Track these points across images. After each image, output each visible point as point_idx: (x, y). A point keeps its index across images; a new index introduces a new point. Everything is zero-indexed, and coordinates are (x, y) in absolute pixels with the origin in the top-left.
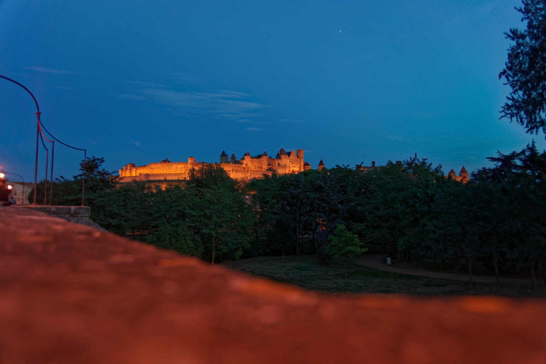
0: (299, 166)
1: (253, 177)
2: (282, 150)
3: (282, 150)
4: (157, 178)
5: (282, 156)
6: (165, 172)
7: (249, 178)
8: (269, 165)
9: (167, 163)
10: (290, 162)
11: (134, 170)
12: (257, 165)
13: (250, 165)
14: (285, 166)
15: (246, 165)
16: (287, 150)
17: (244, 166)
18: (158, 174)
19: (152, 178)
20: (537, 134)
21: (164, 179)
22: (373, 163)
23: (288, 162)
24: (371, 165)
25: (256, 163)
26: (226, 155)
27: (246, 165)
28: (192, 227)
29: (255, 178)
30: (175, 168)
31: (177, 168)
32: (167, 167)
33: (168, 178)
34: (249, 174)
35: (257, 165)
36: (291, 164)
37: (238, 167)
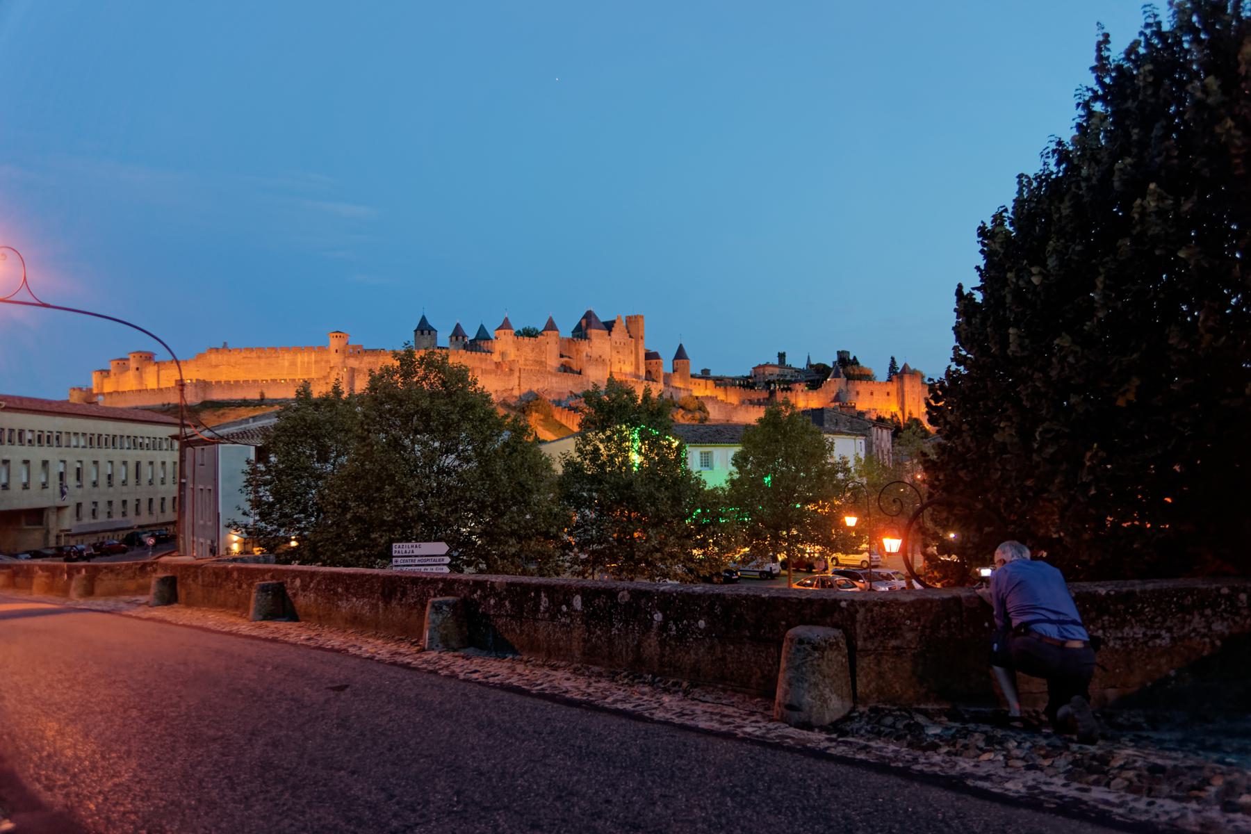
0: (633, 358)
1: (525, 388)
2: (589, 316)
3: (589, 316)
4: (238, 395)
5: (593, 333)
6: (259, 376)
7: (516, 393)
8: (562, 356)
9: (113, 527)
10: (612, 348)
11: (151, 371)
12: (531, 356)
13: (512, 354)
14: (600, 361)
15: (503, 354)
16: (603, 317)
17: (496, 358)
18: (237, 382)
19: (217, 395)
20: (95, 503)
21: (258, 397)
22: (782, 356)
23: (607, 347)
24: (776, 362)
25: (528, 349)
26: (431, 330)
27: (503, 354)
28: (1162, 769)
29: (530, 392)
30: (287, 364)
31: (293, 364)
32: (262, 362)
33: (270, 395)
34: (514, 382)
35: (531, 356)
36: (614, 353)
37: (481, 360)
